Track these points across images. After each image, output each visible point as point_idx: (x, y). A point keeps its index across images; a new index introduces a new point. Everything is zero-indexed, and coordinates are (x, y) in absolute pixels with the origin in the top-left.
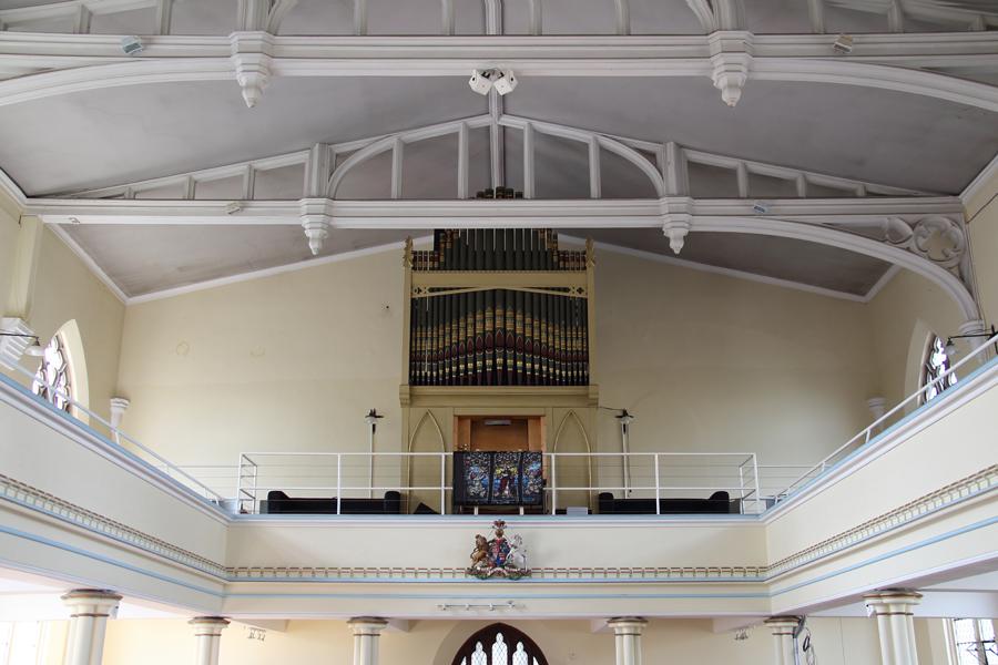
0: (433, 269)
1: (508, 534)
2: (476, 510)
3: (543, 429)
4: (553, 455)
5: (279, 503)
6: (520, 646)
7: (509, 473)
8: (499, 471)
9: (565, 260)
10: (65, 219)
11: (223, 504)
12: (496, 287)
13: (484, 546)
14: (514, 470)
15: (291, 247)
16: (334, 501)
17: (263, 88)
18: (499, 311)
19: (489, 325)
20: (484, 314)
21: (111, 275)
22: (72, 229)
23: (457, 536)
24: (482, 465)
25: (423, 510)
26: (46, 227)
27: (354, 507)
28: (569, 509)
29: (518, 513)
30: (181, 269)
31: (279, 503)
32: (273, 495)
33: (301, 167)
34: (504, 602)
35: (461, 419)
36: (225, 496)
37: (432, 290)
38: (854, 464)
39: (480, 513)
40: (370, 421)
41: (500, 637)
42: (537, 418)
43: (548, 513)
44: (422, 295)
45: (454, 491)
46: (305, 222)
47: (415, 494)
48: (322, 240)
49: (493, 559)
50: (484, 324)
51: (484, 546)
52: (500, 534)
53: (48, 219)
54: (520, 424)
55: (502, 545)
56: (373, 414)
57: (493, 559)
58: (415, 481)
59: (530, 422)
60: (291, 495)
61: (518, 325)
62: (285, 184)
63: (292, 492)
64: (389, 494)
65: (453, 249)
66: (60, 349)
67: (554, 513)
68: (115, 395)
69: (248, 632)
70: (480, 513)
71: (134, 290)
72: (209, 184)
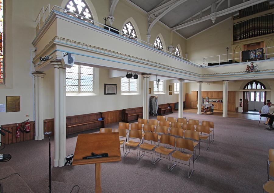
0: (238, 18)
1: (254, 65)
2: (247, 61)
3: (264, 43)
4: (266, 48)
5: (210, 64)
6: (259, 84)
7: (259, 54)
8: (257, 54)
9: (271, 7)
10: (175, 30)
11: (201, 66)
12: (250, 19)
13: (249, 67)
14: (261, 53)
15: (209, 23)
16: (220, 64)
17: (77, 122)
18: (261, 22)
19: (258, 25)
20: (255, 22)
21: (184, 36)
22: (177, 31)
23: (242, 67)
24: (254, 53)
25: (236, 62)
26: (174, 32)
27: (222, 64)
28: (270, 58)
29: (257, 60)
30: (193, 32)
31: (210, 64)
32: (209, 63)
33: (210, 8)
34: (253, 76)
35: (244, 45)
36: (201, 65)
37: (238, 23)
38: (113, 35)
39: (248, 61)
40: (227, 50)
41: (254, 83)
42: (263, 42)
43: (265, 59)
44: (235, 24)
45: (242, 58)
46: (211, 18)
47: (235, 60)
48: (215, 20)
49: (251, 69)
50: (250, 26)
51: (249, 67)
52: (252, 65)
53: (173, 30)
54: (259, 44)
55: (253, 66)
56: (227, 48)
57: (251, 69)
58: (235, 58)
59: (261, 43)
60: (212, 63)
61: (258, 24)
62: (208, 12)
63: (212, 63)
64: (229, 61)
65: (243, 13)
66: (178, 48)
67: (266, 59)
68: (186, 53)
69: (207, 84)
70: (248, 61)
71: (187, 38)
72: (195, 17)
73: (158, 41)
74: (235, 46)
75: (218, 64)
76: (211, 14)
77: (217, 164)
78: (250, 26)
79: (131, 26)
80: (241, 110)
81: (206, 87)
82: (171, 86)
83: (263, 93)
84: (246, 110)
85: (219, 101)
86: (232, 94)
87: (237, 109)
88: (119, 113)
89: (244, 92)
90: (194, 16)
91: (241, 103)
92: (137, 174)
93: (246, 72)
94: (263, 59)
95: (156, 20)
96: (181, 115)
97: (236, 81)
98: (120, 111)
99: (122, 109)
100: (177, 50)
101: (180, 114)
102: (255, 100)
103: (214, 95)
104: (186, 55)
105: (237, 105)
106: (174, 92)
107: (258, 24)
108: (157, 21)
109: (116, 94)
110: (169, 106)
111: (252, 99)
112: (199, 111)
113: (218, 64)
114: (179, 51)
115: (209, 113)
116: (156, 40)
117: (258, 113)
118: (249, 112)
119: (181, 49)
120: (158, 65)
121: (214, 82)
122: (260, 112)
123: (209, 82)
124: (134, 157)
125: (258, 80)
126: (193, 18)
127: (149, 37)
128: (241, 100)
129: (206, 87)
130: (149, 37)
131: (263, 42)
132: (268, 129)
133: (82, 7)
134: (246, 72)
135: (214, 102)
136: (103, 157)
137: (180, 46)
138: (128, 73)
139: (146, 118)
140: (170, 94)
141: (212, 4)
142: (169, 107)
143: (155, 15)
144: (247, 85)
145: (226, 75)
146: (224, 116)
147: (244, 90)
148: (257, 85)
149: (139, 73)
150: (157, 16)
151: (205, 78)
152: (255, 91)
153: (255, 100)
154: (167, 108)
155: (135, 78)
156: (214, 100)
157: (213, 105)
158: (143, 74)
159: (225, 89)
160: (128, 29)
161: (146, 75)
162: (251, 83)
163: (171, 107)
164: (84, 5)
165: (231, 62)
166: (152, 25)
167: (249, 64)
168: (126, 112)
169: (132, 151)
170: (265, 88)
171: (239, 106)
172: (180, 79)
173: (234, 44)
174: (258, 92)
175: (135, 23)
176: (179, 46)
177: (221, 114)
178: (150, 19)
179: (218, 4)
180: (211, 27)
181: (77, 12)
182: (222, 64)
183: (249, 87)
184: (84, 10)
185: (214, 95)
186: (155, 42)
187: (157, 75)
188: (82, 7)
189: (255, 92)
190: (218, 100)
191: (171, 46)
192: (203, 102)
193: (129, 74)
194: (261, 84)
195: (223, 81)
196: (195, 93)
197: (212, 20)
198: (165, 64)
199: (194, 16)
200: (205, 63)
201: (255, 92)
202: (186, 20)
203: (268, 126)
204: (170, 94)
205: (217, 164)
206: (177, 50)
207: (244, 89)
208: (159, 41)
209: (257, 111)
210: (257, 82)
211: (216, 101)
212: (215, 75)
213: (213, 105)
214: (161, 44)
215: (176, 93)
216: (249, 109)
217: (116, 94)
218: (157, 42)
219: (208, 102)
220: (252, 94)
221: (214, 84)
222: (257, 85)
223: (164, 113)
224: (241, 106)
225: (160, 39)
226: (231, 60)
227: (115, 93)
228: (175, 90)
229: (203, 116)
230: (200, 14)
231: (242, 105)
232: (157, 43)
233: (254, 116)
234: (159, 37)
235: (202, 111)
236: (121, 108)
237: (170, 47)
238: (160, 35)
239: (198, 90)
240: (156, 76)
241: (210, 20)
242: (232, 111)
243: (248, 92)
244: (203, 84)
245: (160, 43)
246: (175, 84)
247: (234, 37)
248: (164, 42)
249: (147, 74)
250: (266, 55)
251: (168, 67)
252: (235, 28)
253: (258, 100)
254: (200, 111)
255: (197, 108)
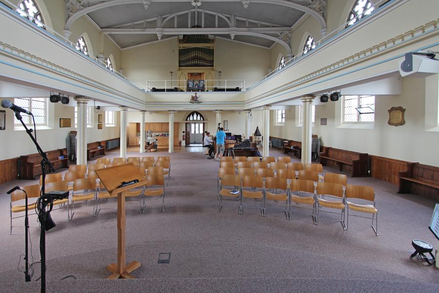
1: (197, 95)
5: (154, 90)
10: (109, 33)
13: (193, 98)
23: (186, 96)
26: (105, 35)
27: (168, 90)
31: (154, 90)
33: (156, 21)
35: (189, 73)
36: (144, 88)
42: (203, 73)
46: (157, 33)
49: (194, 100)
50: (193, 54)
54: (200, 74)
57: (194, 100)
61: (200, 55)
62: (153, 25)
63: (157, 88)
68: (121, 69)
71: (122, 48)
73: (82, 44)
74: (180, 72)
75: (163, 90)
76: (157, 29)
77: (180, 194)
78: (193, 54)
79: (34, 8)
80: (183, 143)
81: (150, 118)
82: (101, 115)
83: (201, 125)
84: (188, 144)
85: (162, 135)
86: (176, 125)
87: (180, 143)
88: (10, 165)
89: (186, 123)
90: (135, 23)
91: (184, 136)
92: (105, 228)
93: (190, 102)
94: (203, 91)
95: (82, 11)
96: (124, 154)
97: (179, 111)
98: (13, 160)
99: (19, 156)
100: (109, 62)
101: (123, 153)
102: (195, 132)
103: (157, 128)
104: (121, 69)
105: (181, 138)
106: (105, 124)
107: (200, 55)
108: (84, 14)
109: (4, 129)
110: (99, 146)
111: (193, 132)
112: (142, 149)
113: (163, 90)
114: (85, 46)
115: (152, 150)
116: (78, 42)
117: (202, 145)
118: (191, 145)
119: (114, 62)
120: (90, 82)
121: (157, 112)
122: (203, 144)
123: (151, 112)
124: (86, 216)
125: (199, 111)
126: (134, 25)
127: (68, 34)
128: (184, 132)
129: (150, 118)
130: (69, 35)
131: (203, 73)
132: (209, 158)
133: (34, 12)
134: (190, 102)
135: (156, 136)
136: (135, 182)
137: (113, 57)
138: (52, 94)
139: (84, 163)
140: (100, 127)
141: (158, 17)
142: (99, 148)
143: (82, 3)
144: (189, 116)
145: (173, 104)
146: (170, 151)
147: (187, 122)
148: (197, 116)
149: (70, 94)
150: (84, 6)
151: (150, 106)
152: (195, 122)
153: (195, 132)
154: (96, 148)
155: (64, 102)
156: (157, 134)
157: (157, 140)
158: (77, 97)
159: (171, 120)
160: (29, 10)
161: (83, 99)
162: (193, 113)
163: (102, 147)
164: (36, 11)
165: (176, 90)
166: (75, 17)
167: (193, 94)
168: (28, 161)
169: (76, 211)
170: (203, 120)
171: (182, 140)
172: (123, 106)
173: (179, 70)
174: (197, 123)
175: (88, 37)
176: (111, 56)
177: (167, 149)
178: (70, 6)
179: (164, 18)
180: (153, 42)
181: (28, 18)
182: (168, 90)
183: (191, 118)
184: (36, 15)
185: (157, 128)
186: (77, 44)
187: (95, 100)
188: (34, 12)
189: (195, 123)
190: (161, 134)
191: (102, 56)
192: (146, 137)
193: (55, 96)
194: (201, 116)
195: (169, 111)
196: (135, 126)
197: (158, 35)
198: (114, 88)
199: (135, 23)
200: (148, 88)
201: (195, 123)
202: (125, 25)
203: (208, 156)
204: (100, 127)
205: (180, 194)
206: (109, 62)
207: (187, 120)
208: (84, 45)
209: (201, 143)
210: (198, 113)
211: (158, 136)
212: (160, 103)
213: (157, 140)
214: (85, 48)
215: (107, 126)
216: (191, 142)
217: (4, 129)
218: (79, 44)
219: (151, 136)
220: (193, 125)
221: (156, 114)
222: (197, 116)
223: (93, 157)
224: (184, 140)
225: (84, 41)
226: (176, 88)
227: (3, 126)
228: (106, 122)
229: (147, 153)
230: (143, 24)
231: (185, 138)
232: (79, 46)
233: (196, 149)
234: (82, 37)
235: (145, 149)
236: (18, 155)
237: (100, 55)
238: (85, 35)
239: (140, 121)
240: (95, 101)
241: (156, 35)
242: (177, 145)
243: (190, 123)
244: (147, 114)
245: (84, 47)
246: (106, 112)
247: (180, 62)
248: (91, 47)
249: (86, 98)
250: (206, 87)
251: (92, 82)
252: (182, 52)
253: (197, 132)
254: (143, 149)
255: (139, 146)
